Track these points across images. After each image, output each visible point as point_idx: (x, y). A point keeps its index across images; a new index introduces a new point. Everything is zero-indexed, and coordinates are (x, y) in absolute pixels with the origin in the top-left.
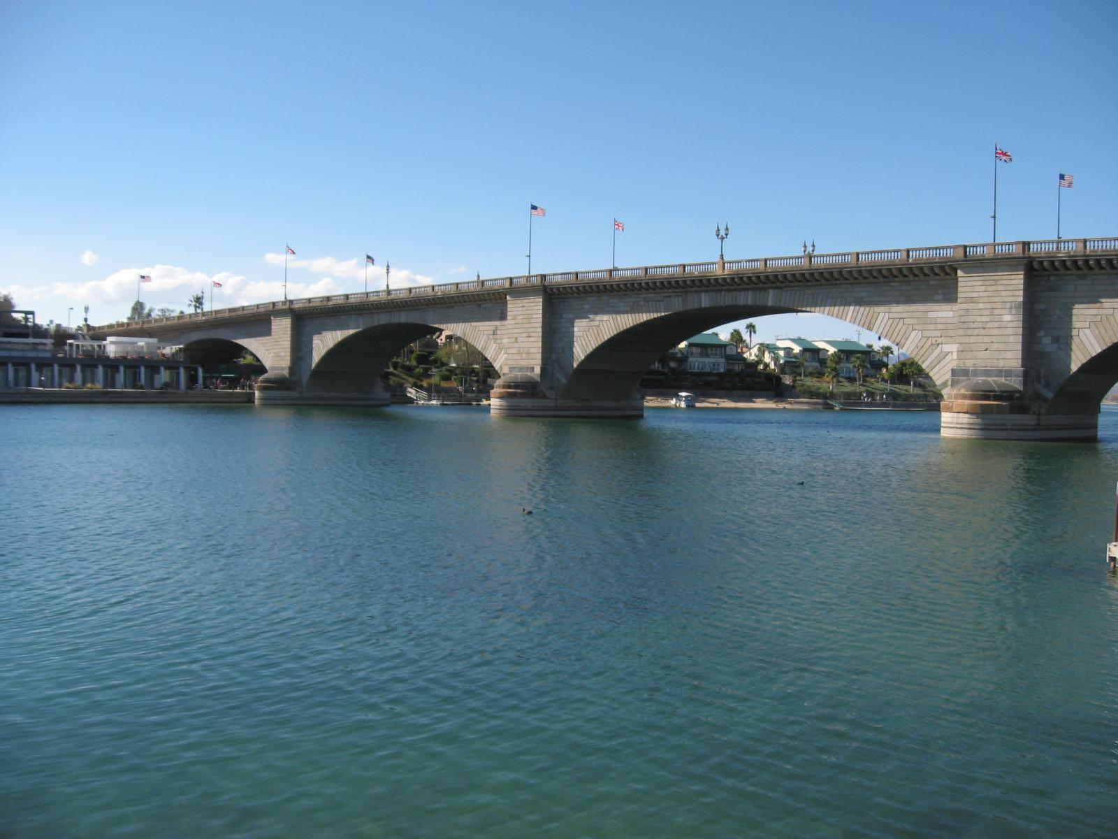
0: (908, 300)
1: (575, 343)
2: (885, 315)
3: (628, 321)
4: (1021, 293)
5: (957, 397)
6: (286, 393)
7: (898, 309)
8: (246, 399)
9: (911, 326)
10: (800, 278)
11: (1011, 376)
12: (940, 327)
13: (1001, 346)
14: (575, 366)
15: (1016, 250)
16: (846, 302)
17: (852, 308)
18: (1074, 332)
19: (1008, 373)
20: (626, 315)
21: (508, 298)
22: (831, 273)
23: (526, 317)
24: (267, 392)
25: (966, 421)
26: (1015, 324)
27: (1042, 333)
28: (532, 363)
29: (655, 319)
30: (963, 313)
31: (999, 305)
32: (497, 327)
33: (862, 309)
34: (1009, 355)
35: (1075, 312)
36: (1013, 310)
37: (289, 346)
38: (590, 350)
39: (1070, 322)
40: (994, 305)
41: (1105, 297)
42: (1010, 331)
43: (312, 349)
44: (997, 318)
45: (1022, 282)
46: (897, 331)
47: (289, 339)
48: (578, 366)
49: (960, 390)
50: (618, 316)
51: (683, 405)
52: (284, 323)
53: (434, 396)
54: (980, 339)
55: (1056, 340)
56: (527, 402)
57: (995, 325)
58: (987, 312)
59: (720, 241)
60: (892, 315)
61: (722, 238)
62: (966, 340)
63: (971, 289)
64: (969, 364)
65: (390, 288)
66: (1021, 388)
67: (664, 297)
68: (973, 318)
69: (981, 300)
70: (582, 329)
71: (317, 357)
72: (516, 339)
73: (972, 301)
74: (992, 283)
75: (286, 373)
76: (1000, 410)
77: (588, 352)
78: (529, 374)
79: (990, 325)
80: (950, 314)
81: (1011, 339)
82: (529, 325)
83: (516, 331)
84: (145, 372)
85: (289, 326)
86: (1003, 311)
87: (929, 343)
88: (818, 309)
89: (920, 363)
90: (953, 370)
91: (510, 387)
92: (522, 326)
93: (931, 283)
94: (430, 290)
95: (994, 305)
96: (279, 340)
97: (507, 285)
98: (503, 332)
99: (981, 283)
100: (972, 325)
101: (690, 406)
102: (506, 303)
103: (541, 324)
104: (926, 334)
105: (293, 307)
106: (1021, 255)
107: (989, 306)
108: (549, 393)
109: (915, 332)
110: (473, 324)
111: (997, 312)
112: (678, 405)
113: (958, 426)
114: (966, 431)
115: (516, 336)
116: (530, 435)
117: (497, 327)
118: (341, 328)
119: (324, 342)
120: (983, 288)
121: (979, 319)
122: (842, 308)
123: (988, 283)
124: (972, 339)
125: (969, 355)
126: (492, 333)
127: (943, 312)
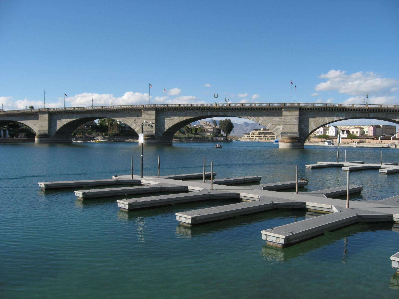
0: (268, 115)
1: (165, 124)
3: (69, 120)
4: (298, 115)
6: (47, 139)
7: (265, 118)
8: (23, 141)
9: (269, 122)
10: (124, 111)
11: (296, 134)
12: (276, 122)
13: (293, 127)
14: (165, 131)
15: (153, 106)
16: (251, 116)
17: (252, 117)
18: (310, 124)
19: (295, 133)
20: (183, 117)
21: (142, 111)
22: (171, 109)
23: (149, 116)
24: (41, 139)
25: (288, 144)
26: (296, 122)
27: (302, 124)
29: (192, 118)
30: (284, 119)
31: (293, 117)
33: (255, 117)
34: (295, 129)
35: (310, 119)
36: (296, 119)
38: (170, 126)
39: (309, 121)
40: (292, 118)
41: (316, 116)
42: (295, 124)
44: (292, 121)
45: (298, 112)
46: (265, 123)
47: (47, 121)
48: (166, 131)
49: (286, 137)
50: (180, 117)
52: (45, 116)
53: (79, 139)
54: (288, 125)
55: (305, 126)
56: (152, 141)
57: (292, 122)
58: (290, 119)
59: (215, 98)
60: (263, 119)
61: (216, 98)
62: (285, 125)
63: (286, 113)
64: (285, 131)
65: (94, 106)
66: (299, 137)
67: (196, 112)
71: (58, 127)
73: (286, 116)
74: (291, 112)
75: (47, 132)
76: (296, 142)
77: (170, 127)
78: (151, 133)
79: (291, 122)
80: (279, 119)
81: (296, 125)
82: (150, 119)
85: (47, 117)
86: (294, 119)
87: (273, 126)
88: (246, 117)
91: (147, 137)
92: (148, 119)
93: (274, 111)
95: (292, 118)
97: (142, 107)
98: (138, 121)
99: (288, 112)
100: (286, 122)
102: (141, 112)
103: (154, 119)
104: (273, 124)
105: (49, 111)
106: (298, 106)
107: (290, 118)
108: (157, 139)
109: (270, 123)
110: (126, 118)
111: (292, 119)
113: (155, 144)
114: (288, 147)
116: (45, 147)
117: (136, 119)
118: (70, 118)
119: (61, 123)
120: (289, 113)
121: (288, 121)
122: (250, 117)
123: (290, 112)
124: (286, 125)
125: (285, 129)
126: (134, 121)
127: (277, 119)
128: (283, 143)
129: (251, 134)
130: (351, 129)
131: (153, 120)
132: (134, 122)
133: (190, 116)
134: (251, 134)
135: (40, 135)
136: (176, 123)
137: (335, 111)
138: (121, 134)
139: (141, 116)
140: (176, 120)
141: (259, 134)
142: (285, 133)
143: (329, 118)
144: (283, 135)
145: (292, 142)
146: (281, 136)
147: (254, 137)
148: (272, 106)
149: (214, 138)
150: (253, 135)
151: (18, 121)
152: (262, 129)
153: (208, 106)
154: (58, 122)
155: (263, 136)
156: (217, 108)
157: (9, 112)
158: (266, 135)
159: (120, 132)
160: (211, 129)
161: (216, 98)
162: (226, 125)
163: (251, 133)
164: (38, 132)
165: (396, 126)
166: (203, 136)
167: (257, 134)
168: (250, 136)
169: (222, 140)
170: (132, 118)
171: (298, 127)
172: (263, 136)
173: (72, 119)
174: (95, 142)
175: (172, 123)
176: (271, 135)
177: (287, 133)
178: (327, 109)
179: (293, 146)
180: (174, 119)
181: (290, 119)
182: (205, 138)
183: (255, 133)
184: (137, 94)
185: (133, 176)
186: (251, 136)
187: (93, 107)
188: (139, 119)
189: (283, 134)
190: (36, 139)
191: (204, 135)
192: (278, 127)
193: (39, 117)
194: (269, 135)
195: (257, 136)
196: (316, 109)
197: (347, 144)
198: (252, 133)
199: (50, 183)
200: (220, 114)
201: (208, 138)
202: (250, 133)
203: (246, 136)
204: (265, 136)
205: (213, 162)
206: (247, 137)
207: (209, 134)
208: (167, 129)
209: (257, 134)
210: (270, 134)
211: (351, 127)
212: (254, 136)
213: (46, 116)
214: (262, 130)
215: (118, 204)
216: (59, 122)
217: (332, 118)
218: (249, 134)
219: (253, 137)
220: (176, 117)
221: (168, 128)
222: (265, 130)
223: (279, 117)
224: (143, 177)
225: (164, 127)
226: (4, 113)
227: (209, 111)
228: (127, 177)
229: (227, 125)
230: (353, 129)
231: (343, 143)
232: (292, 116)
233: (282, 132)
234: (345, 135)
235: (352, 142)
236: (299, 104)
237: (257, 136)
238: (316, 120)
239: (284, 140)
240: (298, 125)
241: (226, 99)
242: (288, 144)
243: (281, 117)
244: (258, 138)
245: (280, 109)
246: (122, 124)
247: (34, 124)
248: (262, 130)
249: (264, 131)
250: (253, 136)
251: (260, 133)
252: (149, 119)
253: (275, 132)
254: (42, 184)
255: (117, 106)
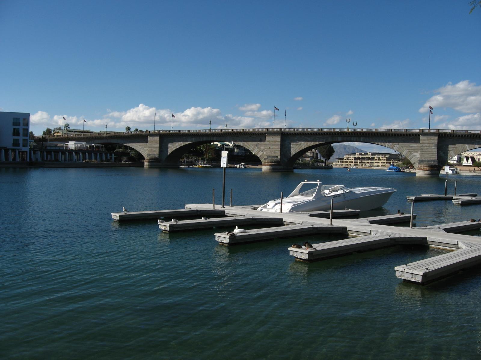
0: (404, 142)
1: (291, 150)
2: (396, 146)
3: (182, 144)
5: (424, 167)
12: (413, 149)
13: (432, 155)
17: (387, 143)
19: (434, 161)
20: (311, 142)
21: (266, 135)
23: (274, 141)
25: (427, 172)
28: (276, 155)
30: (421, 146)
31: (431, 144)
32: (258, 143)
34: (434, 156)
35: (449, 146)
37: (158, 147)
38: (297, 151)
42: (434, 151)
43: (168, 148)
48: (292, 156)
49: (424, 165)
50: (308, 142)
51: (243, 167)
55: (444, 153)
58: (428, 146)
61: (348, 122)
63: (424, 140)
64: (423, 158)
65: (211, 129)
66: (437, 165)
68: (424, 147)
69: (427, 143)
70: (293, 145)
71: (170, 151)
72: (270, 147)
73: (424, 143)
75: (157, 156)
77: (296, 152)
81: (434, 153)
82: (275, 144)
83: (270, 145)
84: (94, 155)
86: (432, 146)
89: (407, 158)
90: (419, 160)
91: (273, 163)
94: (122, 133)
96: (152, 144)
97: (266, 131)
99: (426, 139)
100: (424, 149)
101: (245, 167)
104: (409, 150)
107: (428, 144)
109: (406, 150)
111: (430, 146)
112: (240, 167)
115: (270, 147)
116: (155, 173)
117: (258, 143)
118: (183, 141)
119: (172, 147)
120: (427, 140)
121: (426, 147)
123: (428, 139)
124: (424, 152)
126: (256, 145)
127: (414, 145)
128: (422, 171)
129: (345, 159)
130: (477, 156)
131: (278, 145)
132: (256, 146)
133: (318, 141)
134: (345, 159)
135: (150, 159)
136: (303, 148)
137: (476, 138)
138: (218, 159)
139: (265, 140)
140: (304, 145)
141: (355, 160)
142: (422, 161)
143: (470, 145)
144: (420, 163)
145: (431, 170)
146: (418, 163)
147: (349, 163)
148: (408, 132)
149: (315, 164)
150: (347, 161)
151: (125, 144)
152: (357, 154)
153: (339, 131)
154: (170, 145)
155: (360, 162)
156: (349, 134)
157: (114, 134)
158: (363, 161)
159: (216, 156)
160: (311, 154)
161: (348, 122)
162: (326, 149)
163: (345, 158)
164: (147, 156)
165: (14, 118)
166: (303, 161)
167: (352, 160)
168: (343, 162)
169: (324, 167)
170: (254, 142)
171: (437, 154)
172: (360, 162)
173: (186, 143)
174: (199, 167)
175: (299, 148)
176: (369, 160)
177: (425, 161)
178: (468, 136)
179: (432, 174)
180: (301, 144)
181: (428, 146)
182: (306, 164)
183: (350, 158)
184: (147, 106)
185: (215, 205)
186: (345, 162)
187: (210, 130)
188: (262, 144)
189: (420, 161)
190: (146, 164)
191: (304, 160)
192: (415, 154)
193: (148, 140)
194: (367, 161)
195: (352, 162)
196: (456, 136)
197: (473, 172)
198: (346, 158)
199: (125, 214)
200: (339, 139)
201: (309, 164)
202: (344, 158)
203: (338, 162)
204: (362, 162)
205: (215, 189)
206: (339, 163)
207: (308, 159)
208: (293, 155)
209: (352, 160)
210: (368, 160)
211: (475, 154)
212: (380, 163)
213: (157, 139)
214: (357, 155)
215: (216, 238)
216: (170, 145)
217: (473, 145)
218: (342, 159)
219: (347, 163)
220: (303, 142)
221: (294, 154)
222: (360, 154)
223: (416, 144)
224: (225, 206)
225: (290, 152)
226: (107, 135)
227: (340, 136)
228: (208, 207)
229: (327, 149)
230: (479, 156)
231: (469, 171)
232: (430, 143)
233: (419, 159)
234: (470, 162)
235: (479, 171)
236: (439, 130)
237: (352, 162)
238: (455, 147)
239: (422, 168)
240: (437, 153)
241: (354, 123)
242: (427, 172)
243: (418, 144)
244: (353, 164)
245: (417, 135)
246: (217, 147)
247: (142, 147)
248: (357, 155)
249: (360, 156)
250: (347, 162)
251: (356, 159)
252: (273, 144)
253: (411, 160)
254: (116, 216)
255: (228, 129)
